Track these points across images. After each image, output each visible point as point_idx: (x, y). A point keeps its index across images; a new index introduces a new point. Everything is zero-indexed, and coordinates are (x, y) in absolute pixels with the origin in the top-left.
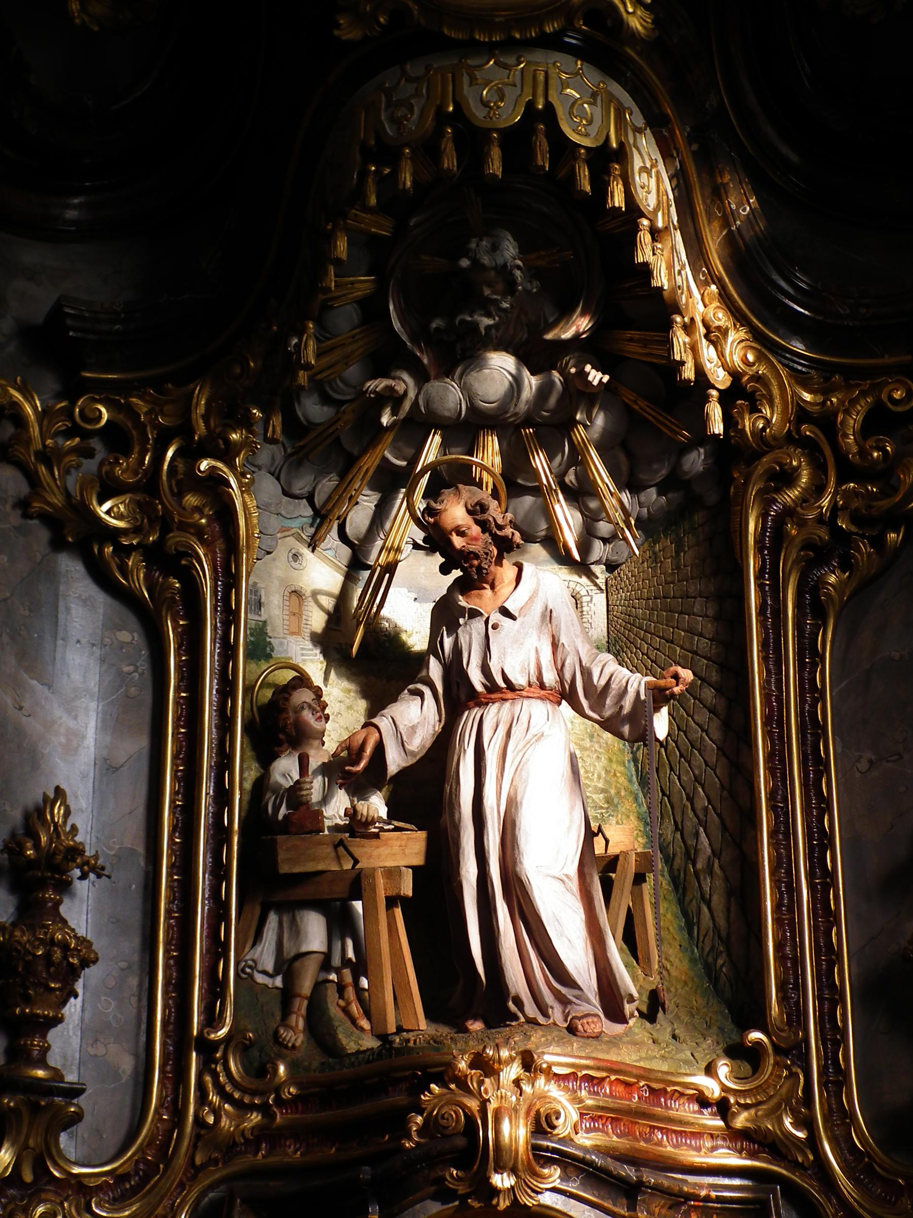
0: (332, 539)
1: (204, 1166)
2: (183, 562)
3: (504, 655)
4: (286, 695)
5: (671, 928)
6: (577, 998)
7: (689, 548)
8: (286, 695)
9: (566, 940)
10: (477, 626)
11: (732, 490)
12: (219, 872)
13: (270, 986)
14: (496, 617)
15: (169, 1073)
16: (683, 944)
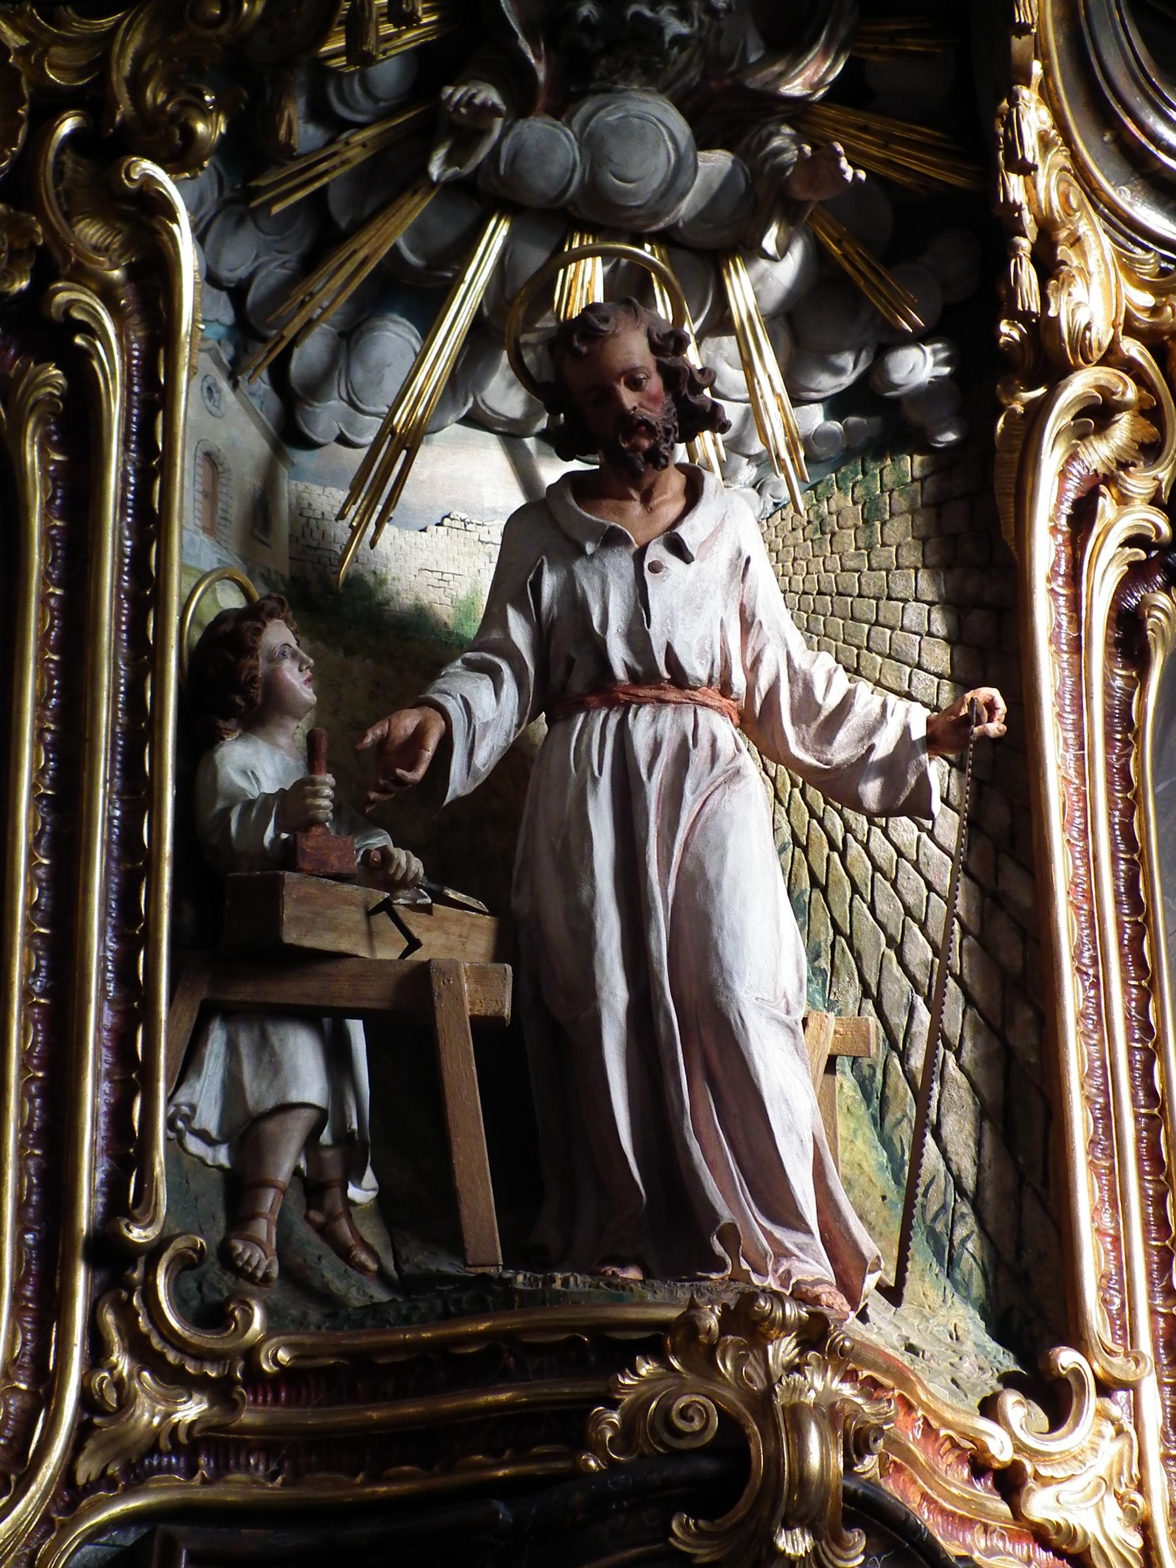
0: (262, 384)
1: (91, 1487)
2: (78, 340)
3: (672, 620)
4: (259, 625)
5: (865, 1165)
6: (801, 1249)
7: (892, 515)
8: (259, 625)
9: (797, 1143)
10: (619, 564)
11: (1000, 424)
12: (132, 929)
13: (210, 1162)
14: (657, 552)
15: (29, 1300)
16: (888, 1195)
